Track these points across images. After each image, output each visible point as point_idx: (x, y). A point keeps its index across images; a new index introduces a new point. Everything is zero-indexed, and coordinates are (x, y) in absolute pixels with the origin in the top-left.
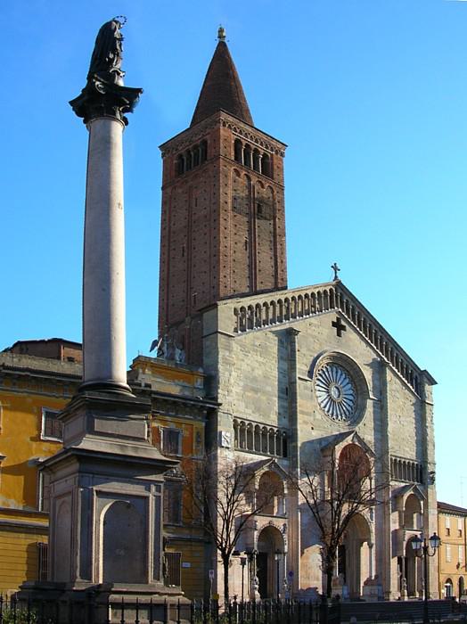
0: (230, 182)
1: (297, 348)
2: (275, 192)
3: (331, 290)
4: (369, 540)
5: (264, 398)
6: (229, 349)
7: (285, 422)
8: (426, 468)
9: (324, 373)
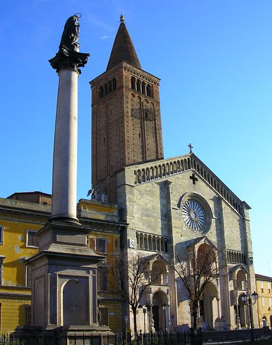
0: (130, 101)
4: (217, 297)
5: (153, 220)
6: (132, 193)
7: (166, 233)
8: (247, 255)
9: (186, 205)
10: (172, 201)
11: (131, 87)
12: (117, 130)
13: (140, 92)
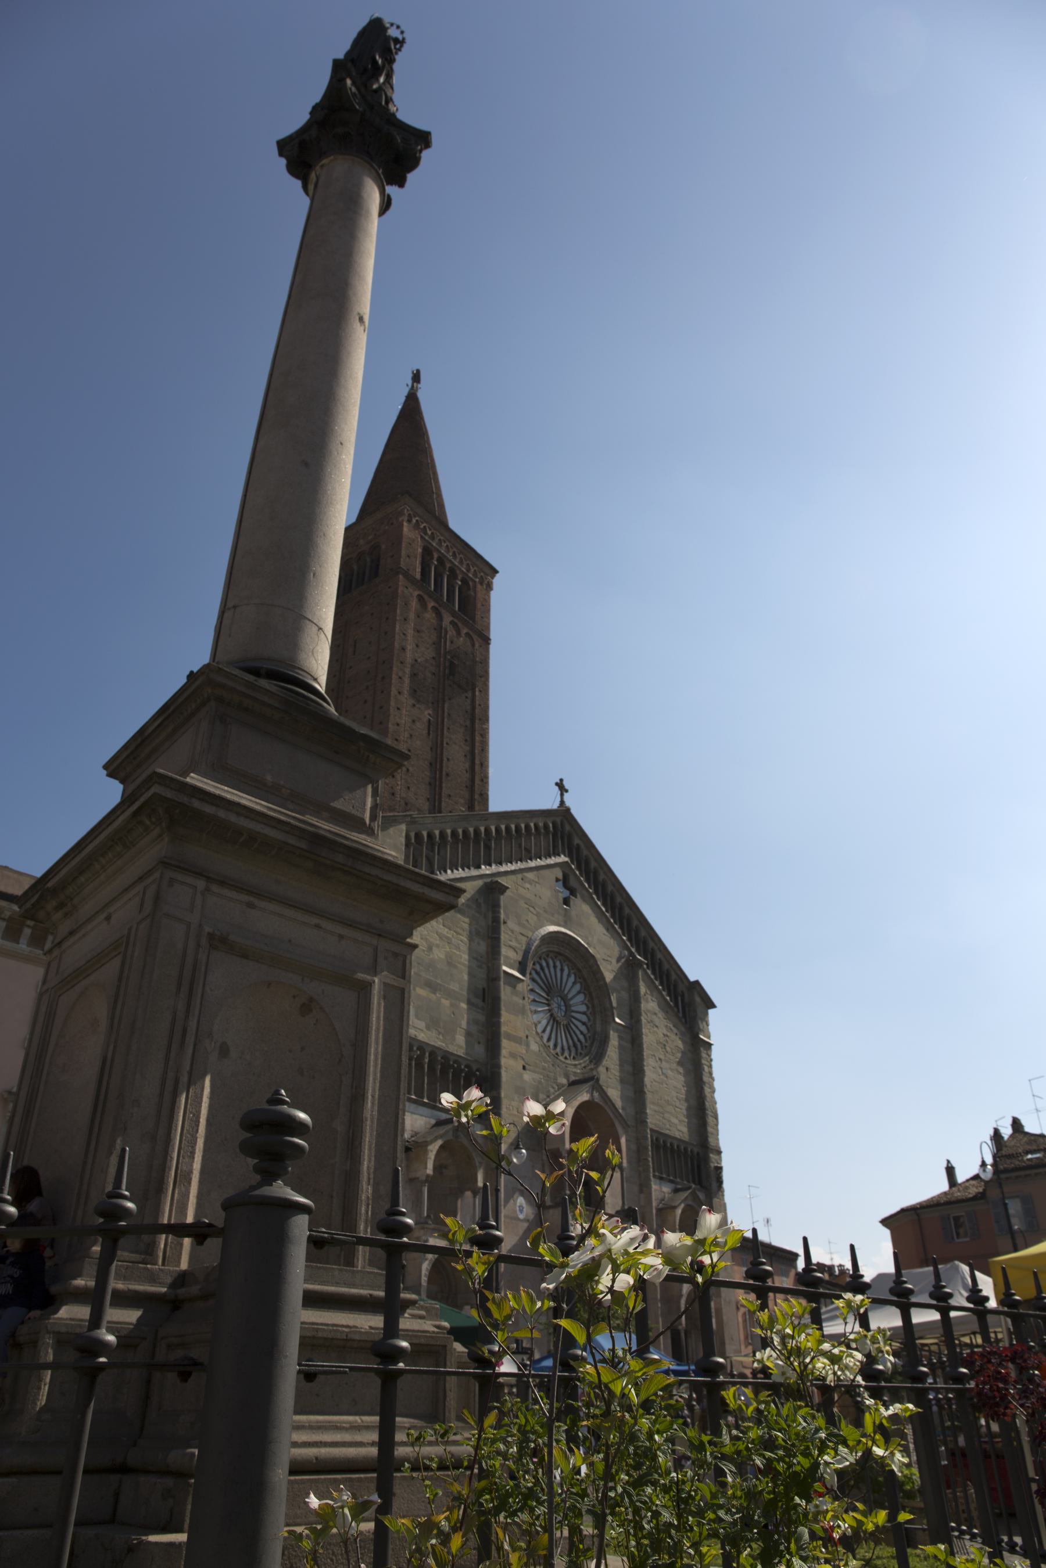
0: (412, 616)
1: (502, 916)
2: (477, 645)
5: (446, 1003)
7: (480, 1051)
8: (707, 1160)
9: (542, 968)
10: (504, 950)
11: (418, 576)
12: (365, 702)
13: (442, 595)
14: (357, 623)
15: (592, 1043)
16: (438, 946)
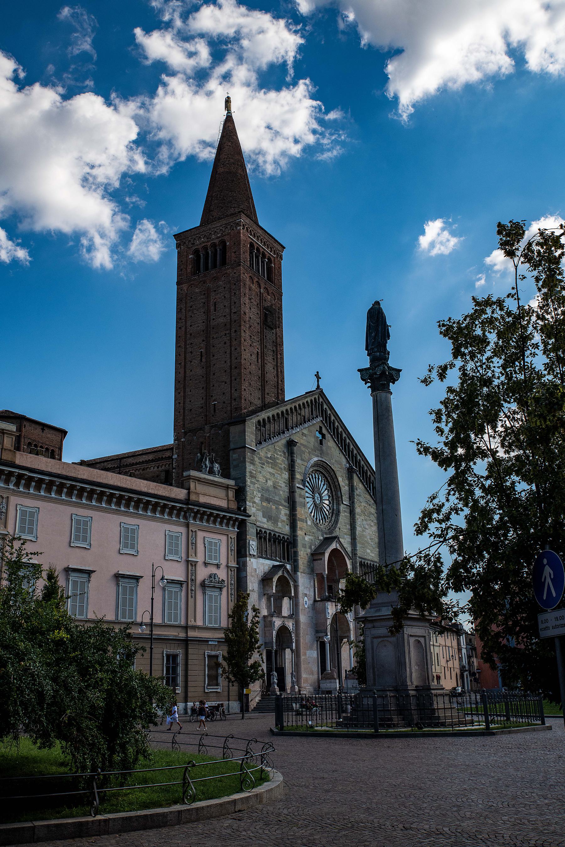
3: (315, 399)
4: (348, 637)
5: (274, 507)
6: (253, 463)
12: (225, 343)
14: (215, 291)
15: (332, 516)
16: (269, 479)
